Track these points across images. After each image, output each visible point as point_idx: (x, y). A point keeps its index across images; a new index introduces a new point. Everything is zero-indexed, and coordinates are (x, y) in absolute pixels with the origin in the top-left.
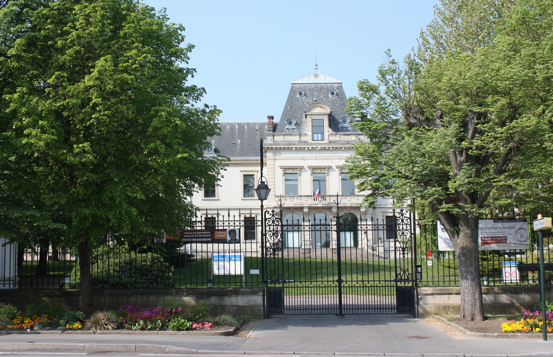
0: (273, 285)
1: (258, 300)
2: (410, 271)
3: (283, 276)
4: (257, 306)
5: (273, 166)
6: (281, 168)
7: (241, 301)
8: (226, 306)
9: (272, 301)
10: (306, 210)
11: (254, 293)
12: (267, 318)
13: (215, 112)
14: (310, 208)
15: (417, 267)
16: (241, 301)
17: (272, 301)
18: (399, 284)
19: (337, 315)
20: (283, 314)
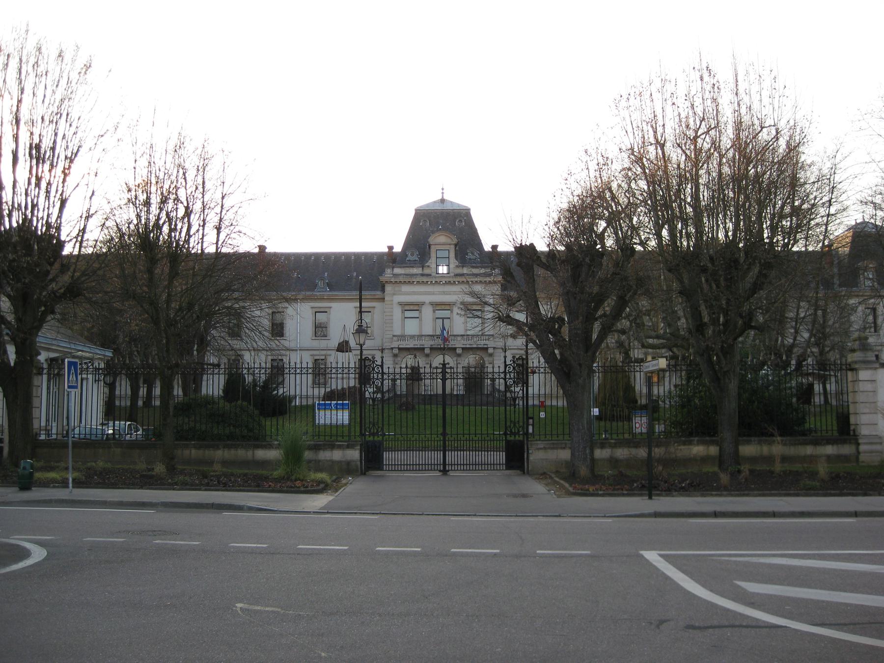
0: (371, 438)
1: (354, 454)
2: (521, 424)
3: (382, 429)
4: (354, 461)
5: (363, 310)
6: (400, 304)
7: (337, 455)
8: (319, 461)
9: (665, 233)
10: (427, 351)
11: (350, 446)
12: (365, 474)
13: (495, 247)
14: (431, 349)
15: (528, 418)
16: (337, 455)
17: (665, 233)
18: (509, 438)
19: (440, 471)
20: (382, 470)
